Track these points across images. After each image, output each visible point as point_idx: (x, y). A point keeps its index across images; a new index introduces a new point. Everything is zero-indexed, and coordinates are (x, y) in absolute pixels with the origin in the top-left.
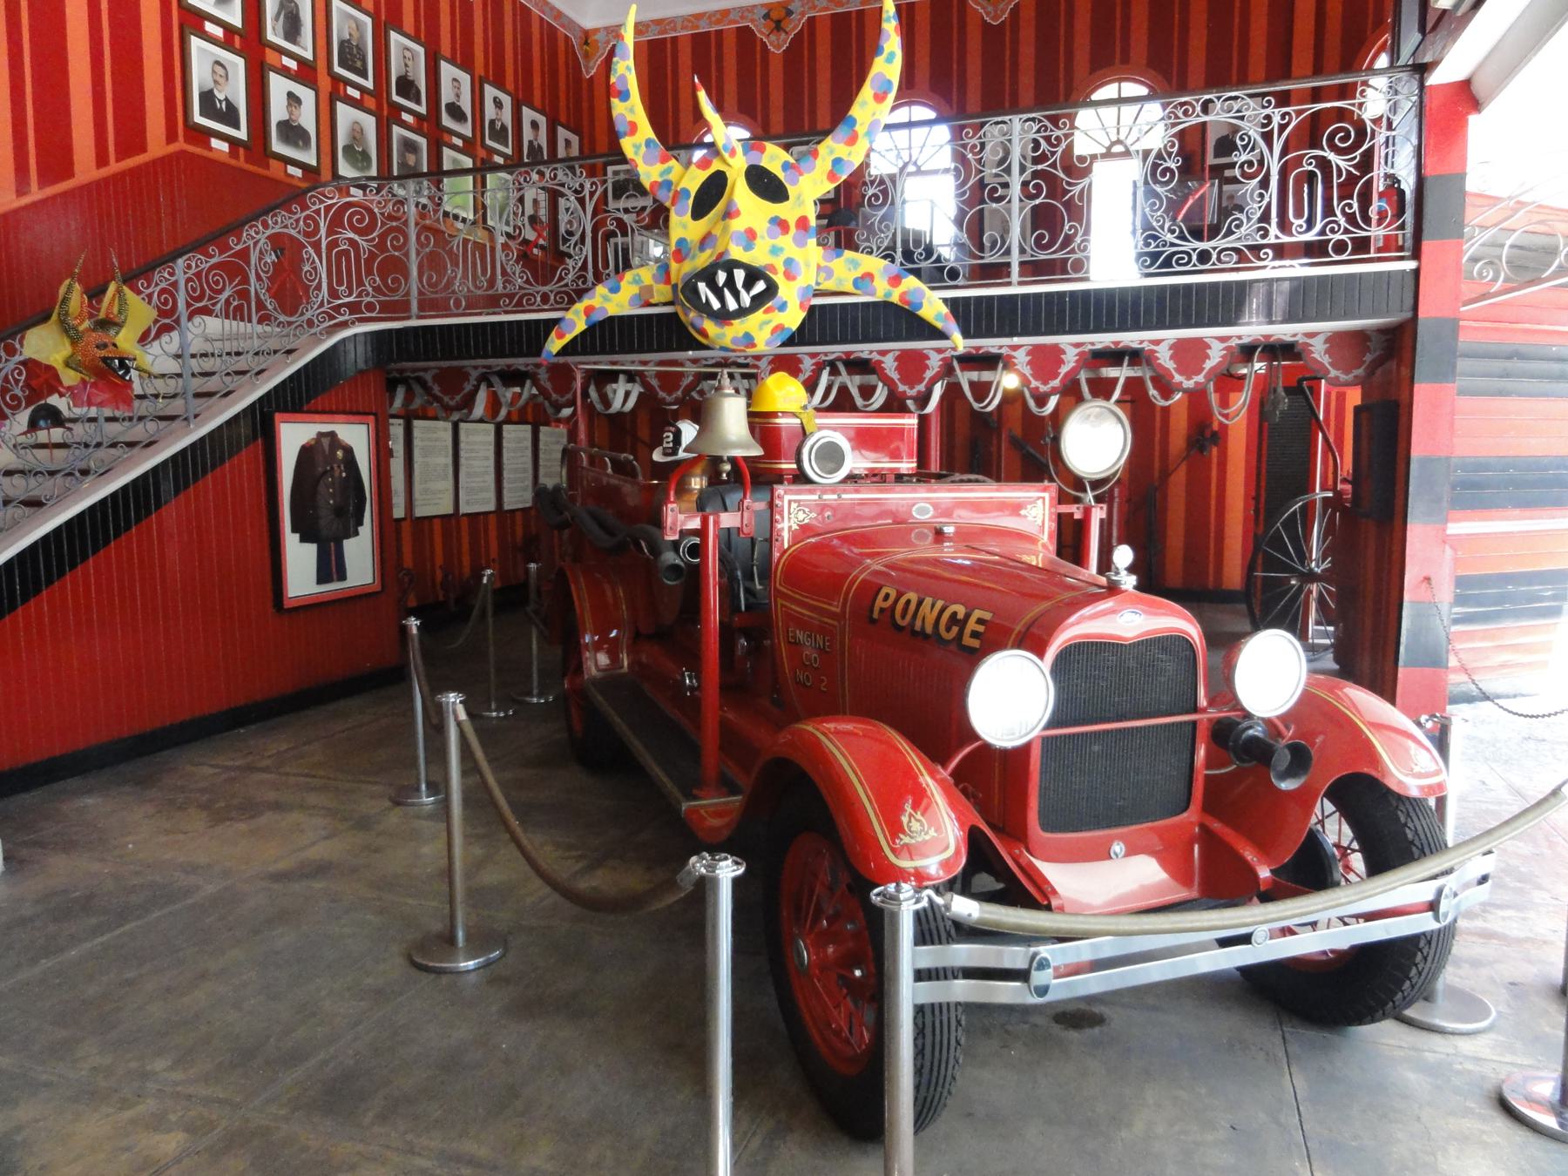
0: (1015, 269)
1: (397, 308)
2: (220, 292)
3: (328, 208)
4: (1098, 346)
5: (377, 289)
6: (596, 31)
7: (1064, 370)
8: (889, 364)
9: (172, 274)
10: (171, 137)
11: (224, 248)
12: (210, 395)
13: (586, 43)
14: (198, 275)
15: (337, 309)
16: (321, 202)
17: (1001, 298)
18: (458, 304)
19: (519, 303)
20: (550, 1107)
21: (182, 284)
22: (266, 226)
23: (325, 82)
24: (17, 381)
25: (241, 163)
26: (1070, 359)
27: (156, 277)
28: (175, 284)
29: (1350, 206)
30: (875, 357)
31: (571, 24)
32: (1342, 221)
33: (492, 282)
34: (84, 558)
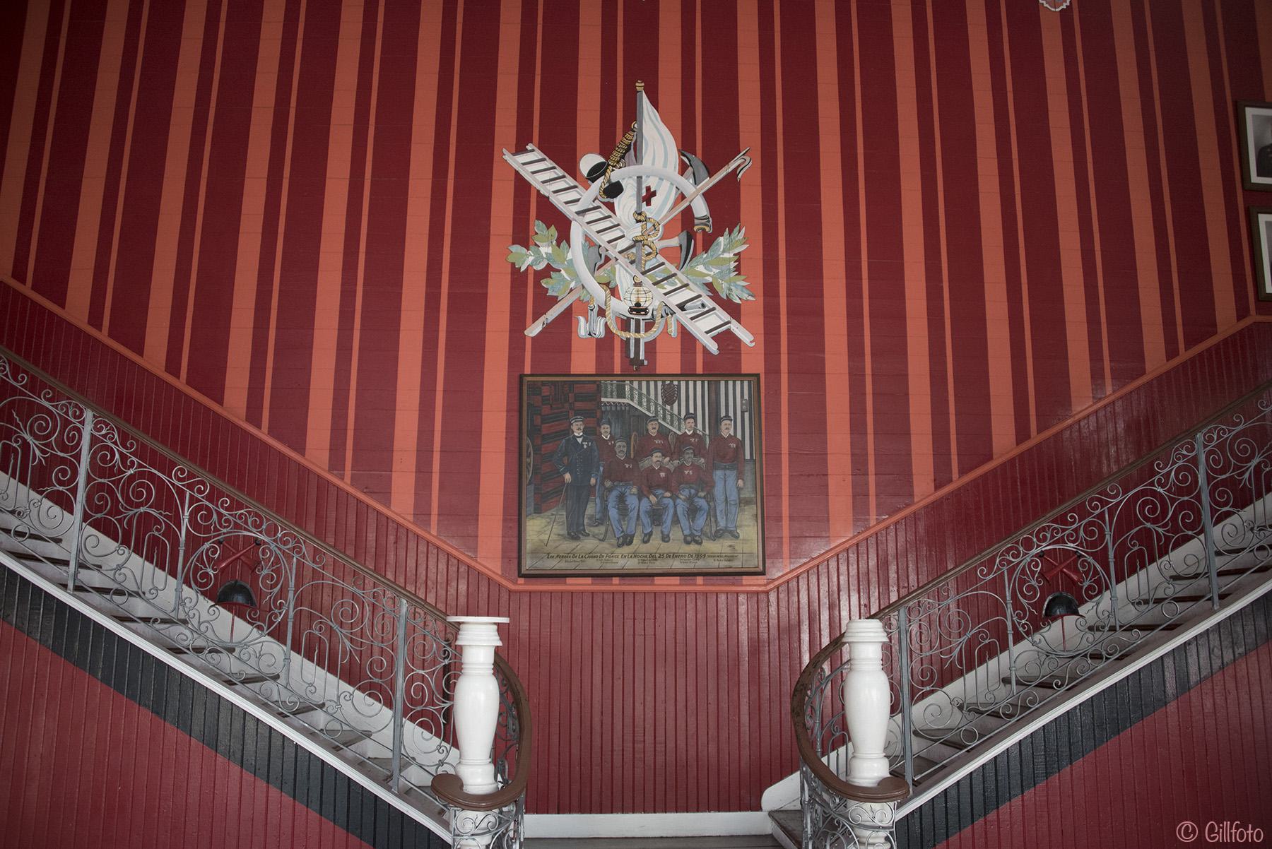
2: (1249, 460)
9: (1192, 449)
10: (1242, 313)
14: (1221, 446)
16: (1104, 503)
20: (636, 242)
21: (1203, 458)
24: (1033, 573)
27: (1173, 456)
28: (1195, 460)
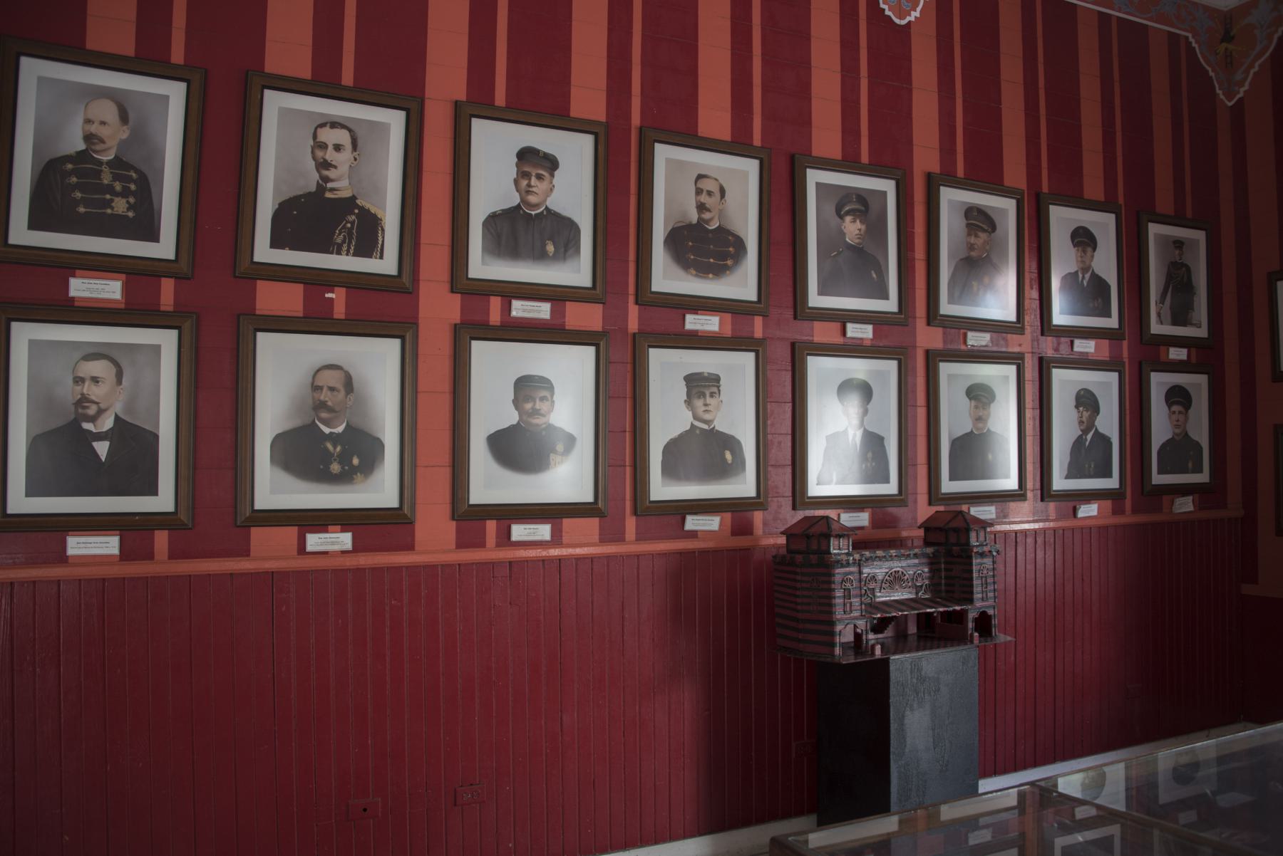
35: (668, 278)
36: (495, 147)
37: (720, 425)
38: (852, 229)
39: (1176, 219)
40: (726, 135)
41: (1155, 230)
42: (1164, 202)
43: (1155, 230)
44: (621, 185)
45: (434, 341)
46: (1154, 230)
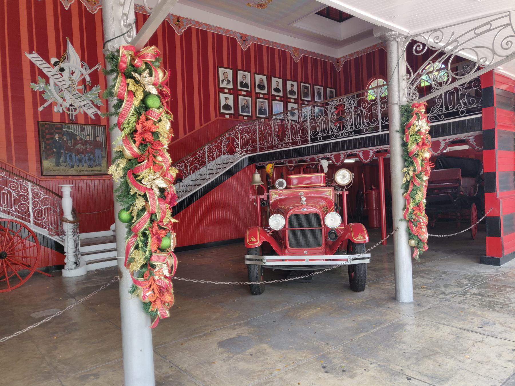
0: (310, 140)
1: (255, 151)
3: (240, 129)
4: (451, 140)
5: (251, 146)
6: (340, 58)
7: (370, 156)
8: (361, 154)
10: (216, 116)
11: (216, 142)
12: (212, 174)
13: (338, 62)
14: (210, 149)
15: (242, 152)
17: (376, 136)
18: (320, 139)
19: (336, 137)
22: (225, 136)
23: (254, 95)
25: (232, 119)
26: (371, 153)
28: (205, 151)
29: (464, 100)
30: (357, 153)
31: (332, 58)
32: (462, 105)
33: (272, 142)
34: (185, 208)
35: (274, 93)
36: (258, 77)
37: (229, 104)
38: (306, 90)
39: (291, 80)
40: (227, 67)
41: (328, 89)
42: (329, 85)
43: (328, 89)
44: (253, 79)
45: (254, 99)
46: (328, 89)
